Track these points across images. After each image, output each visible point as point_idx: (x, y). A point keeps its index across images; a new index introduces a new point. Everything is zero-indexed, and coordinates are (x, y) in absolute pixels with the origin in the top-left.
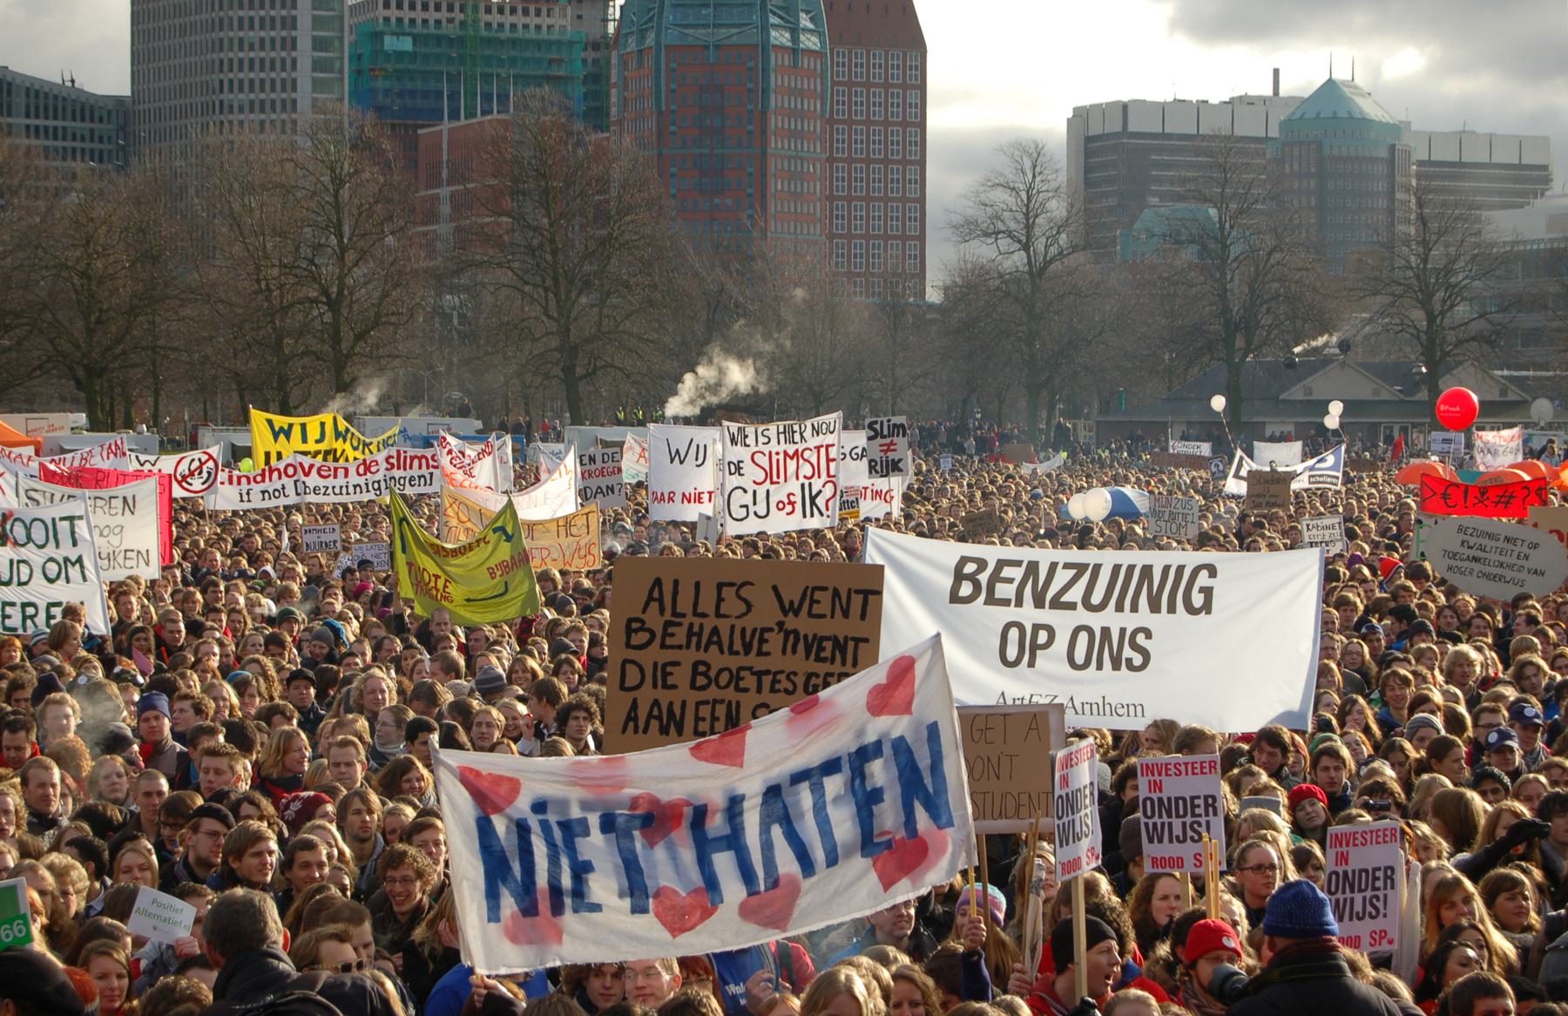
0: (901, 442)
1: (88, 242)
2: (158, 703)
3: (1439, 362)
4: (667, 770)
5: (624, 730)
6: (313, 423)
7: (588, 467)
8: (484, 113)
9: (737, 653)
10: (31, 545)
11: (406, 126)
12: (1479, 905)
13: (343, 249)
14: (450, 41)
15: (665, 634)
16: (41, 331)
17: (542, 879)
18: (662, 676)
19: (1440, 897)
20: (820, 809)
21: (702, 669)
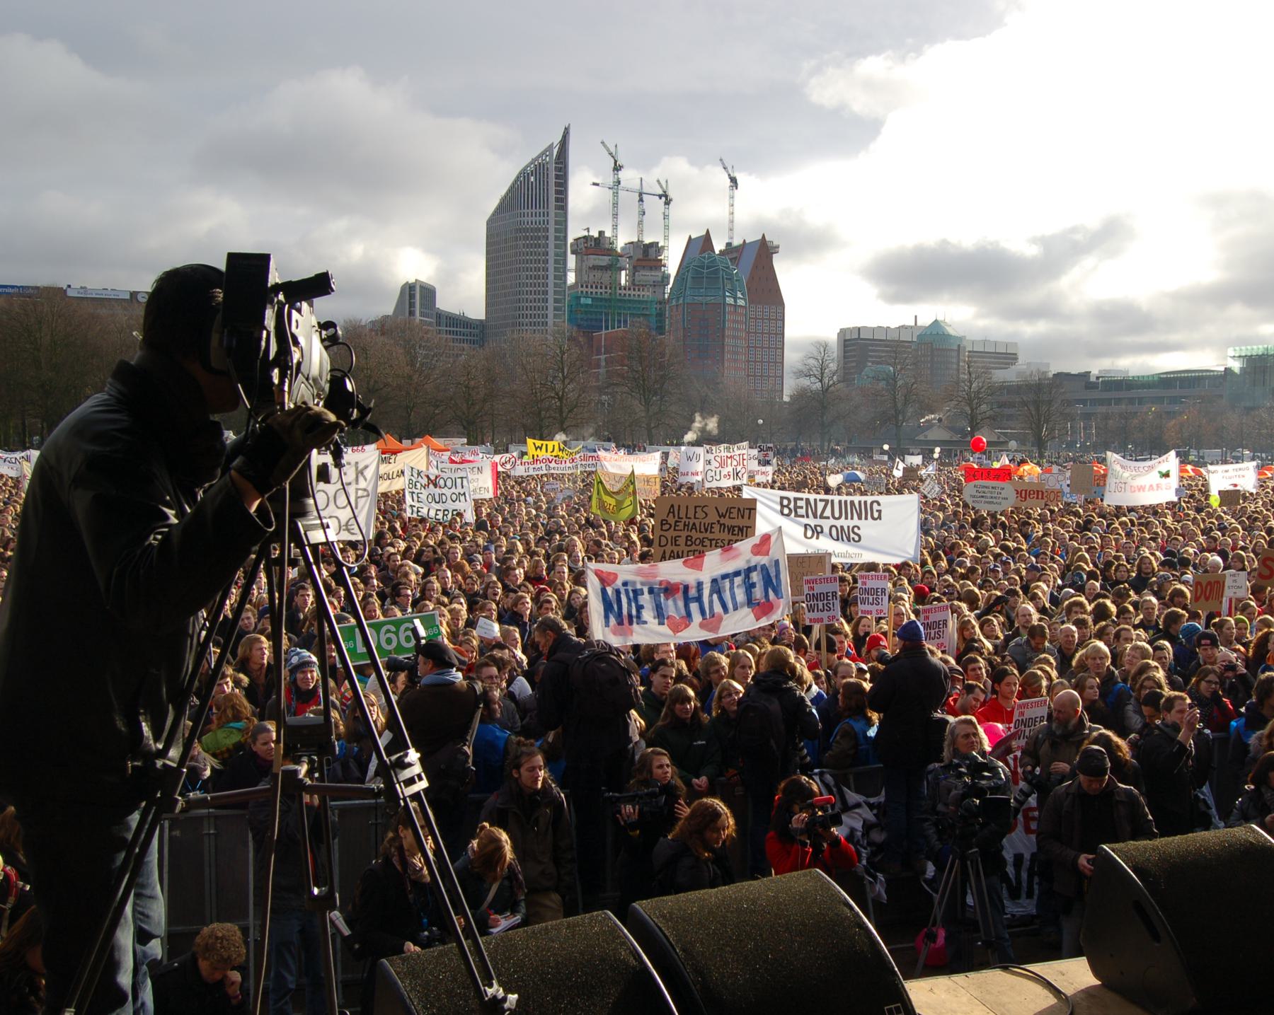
0: (771, 454)
3: (975, 427)
4: (672, 570)
6: (550, 444)
12: (977, 629)
13: (564, 378)
14: (606, 300)
17: (625, 611)
18: (675, 541)
19: (964, 626)
20: (732, 588)
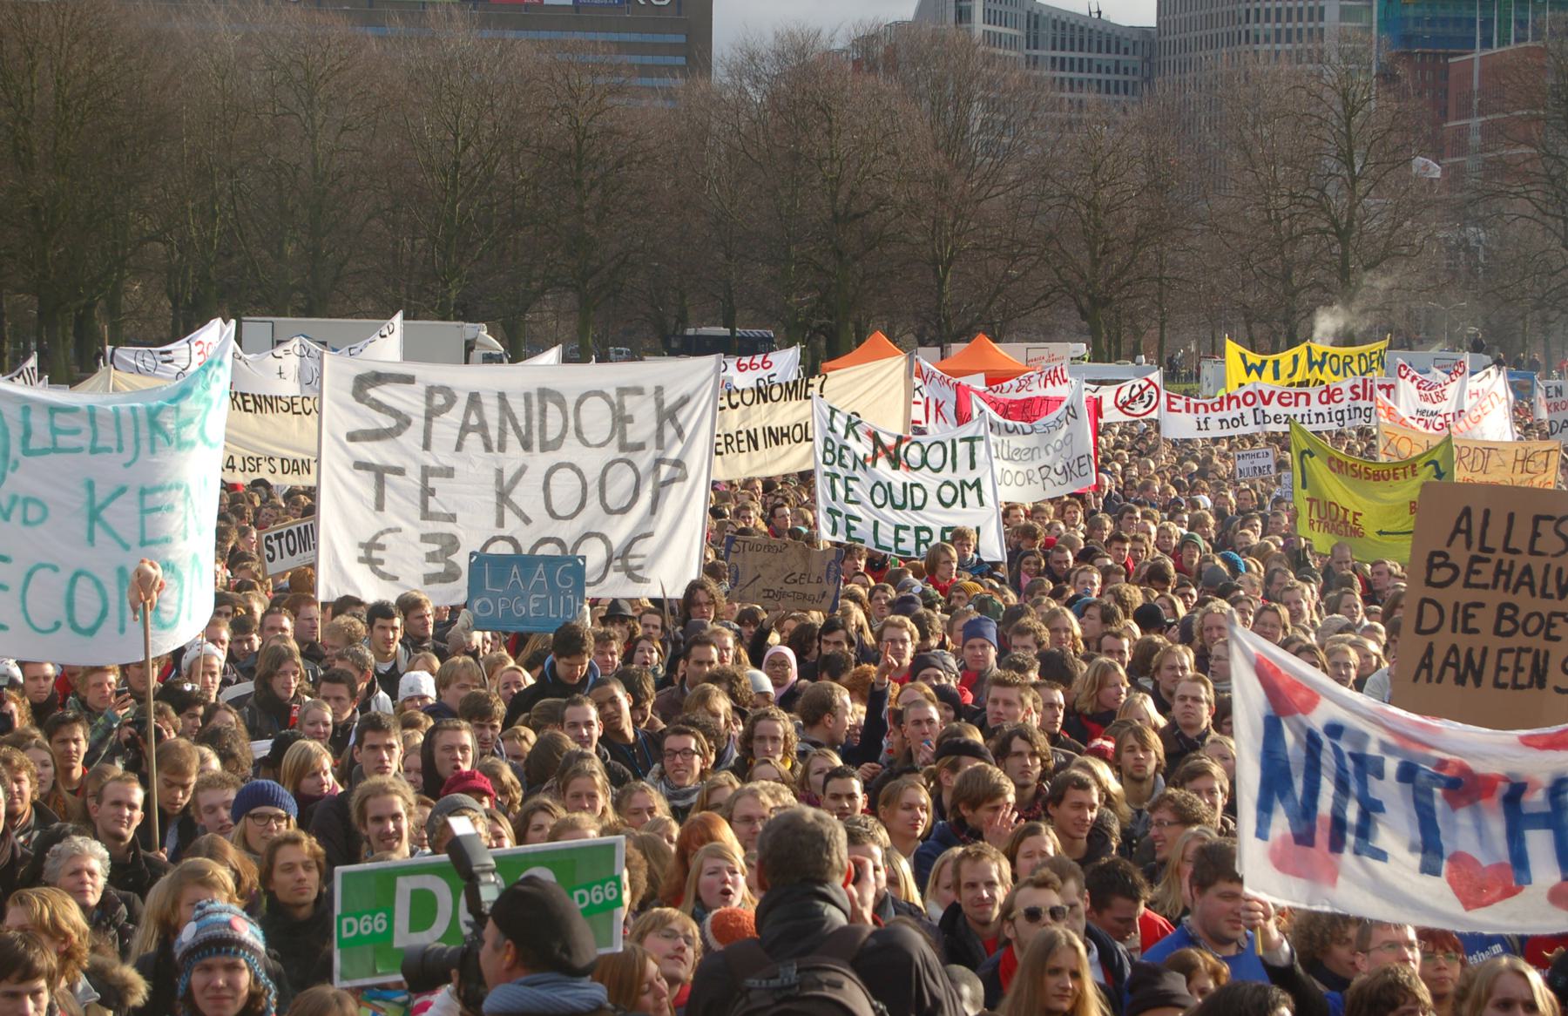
1: (1095, 171)
2: (986, 631)
5: (1416, 679)
6: (1285, 358)
7: (1554, 400)
8: (1517, 40)
9: (1550, 596)
10: (925, 468)
11: (1437, 55)
15: (1471, 571)
16: (1046, 260)
18: (1464, 617)
21: (1508, 612)
